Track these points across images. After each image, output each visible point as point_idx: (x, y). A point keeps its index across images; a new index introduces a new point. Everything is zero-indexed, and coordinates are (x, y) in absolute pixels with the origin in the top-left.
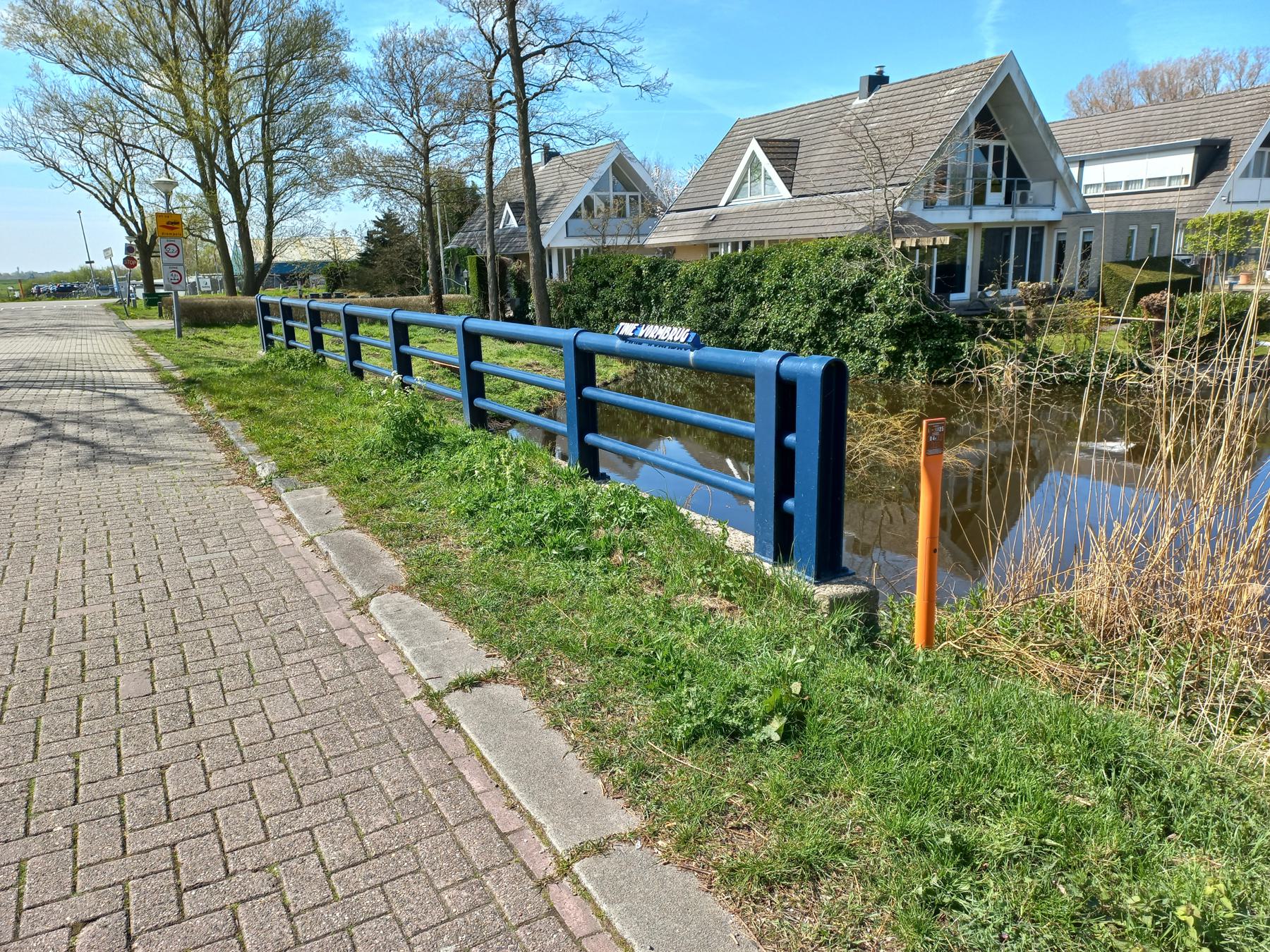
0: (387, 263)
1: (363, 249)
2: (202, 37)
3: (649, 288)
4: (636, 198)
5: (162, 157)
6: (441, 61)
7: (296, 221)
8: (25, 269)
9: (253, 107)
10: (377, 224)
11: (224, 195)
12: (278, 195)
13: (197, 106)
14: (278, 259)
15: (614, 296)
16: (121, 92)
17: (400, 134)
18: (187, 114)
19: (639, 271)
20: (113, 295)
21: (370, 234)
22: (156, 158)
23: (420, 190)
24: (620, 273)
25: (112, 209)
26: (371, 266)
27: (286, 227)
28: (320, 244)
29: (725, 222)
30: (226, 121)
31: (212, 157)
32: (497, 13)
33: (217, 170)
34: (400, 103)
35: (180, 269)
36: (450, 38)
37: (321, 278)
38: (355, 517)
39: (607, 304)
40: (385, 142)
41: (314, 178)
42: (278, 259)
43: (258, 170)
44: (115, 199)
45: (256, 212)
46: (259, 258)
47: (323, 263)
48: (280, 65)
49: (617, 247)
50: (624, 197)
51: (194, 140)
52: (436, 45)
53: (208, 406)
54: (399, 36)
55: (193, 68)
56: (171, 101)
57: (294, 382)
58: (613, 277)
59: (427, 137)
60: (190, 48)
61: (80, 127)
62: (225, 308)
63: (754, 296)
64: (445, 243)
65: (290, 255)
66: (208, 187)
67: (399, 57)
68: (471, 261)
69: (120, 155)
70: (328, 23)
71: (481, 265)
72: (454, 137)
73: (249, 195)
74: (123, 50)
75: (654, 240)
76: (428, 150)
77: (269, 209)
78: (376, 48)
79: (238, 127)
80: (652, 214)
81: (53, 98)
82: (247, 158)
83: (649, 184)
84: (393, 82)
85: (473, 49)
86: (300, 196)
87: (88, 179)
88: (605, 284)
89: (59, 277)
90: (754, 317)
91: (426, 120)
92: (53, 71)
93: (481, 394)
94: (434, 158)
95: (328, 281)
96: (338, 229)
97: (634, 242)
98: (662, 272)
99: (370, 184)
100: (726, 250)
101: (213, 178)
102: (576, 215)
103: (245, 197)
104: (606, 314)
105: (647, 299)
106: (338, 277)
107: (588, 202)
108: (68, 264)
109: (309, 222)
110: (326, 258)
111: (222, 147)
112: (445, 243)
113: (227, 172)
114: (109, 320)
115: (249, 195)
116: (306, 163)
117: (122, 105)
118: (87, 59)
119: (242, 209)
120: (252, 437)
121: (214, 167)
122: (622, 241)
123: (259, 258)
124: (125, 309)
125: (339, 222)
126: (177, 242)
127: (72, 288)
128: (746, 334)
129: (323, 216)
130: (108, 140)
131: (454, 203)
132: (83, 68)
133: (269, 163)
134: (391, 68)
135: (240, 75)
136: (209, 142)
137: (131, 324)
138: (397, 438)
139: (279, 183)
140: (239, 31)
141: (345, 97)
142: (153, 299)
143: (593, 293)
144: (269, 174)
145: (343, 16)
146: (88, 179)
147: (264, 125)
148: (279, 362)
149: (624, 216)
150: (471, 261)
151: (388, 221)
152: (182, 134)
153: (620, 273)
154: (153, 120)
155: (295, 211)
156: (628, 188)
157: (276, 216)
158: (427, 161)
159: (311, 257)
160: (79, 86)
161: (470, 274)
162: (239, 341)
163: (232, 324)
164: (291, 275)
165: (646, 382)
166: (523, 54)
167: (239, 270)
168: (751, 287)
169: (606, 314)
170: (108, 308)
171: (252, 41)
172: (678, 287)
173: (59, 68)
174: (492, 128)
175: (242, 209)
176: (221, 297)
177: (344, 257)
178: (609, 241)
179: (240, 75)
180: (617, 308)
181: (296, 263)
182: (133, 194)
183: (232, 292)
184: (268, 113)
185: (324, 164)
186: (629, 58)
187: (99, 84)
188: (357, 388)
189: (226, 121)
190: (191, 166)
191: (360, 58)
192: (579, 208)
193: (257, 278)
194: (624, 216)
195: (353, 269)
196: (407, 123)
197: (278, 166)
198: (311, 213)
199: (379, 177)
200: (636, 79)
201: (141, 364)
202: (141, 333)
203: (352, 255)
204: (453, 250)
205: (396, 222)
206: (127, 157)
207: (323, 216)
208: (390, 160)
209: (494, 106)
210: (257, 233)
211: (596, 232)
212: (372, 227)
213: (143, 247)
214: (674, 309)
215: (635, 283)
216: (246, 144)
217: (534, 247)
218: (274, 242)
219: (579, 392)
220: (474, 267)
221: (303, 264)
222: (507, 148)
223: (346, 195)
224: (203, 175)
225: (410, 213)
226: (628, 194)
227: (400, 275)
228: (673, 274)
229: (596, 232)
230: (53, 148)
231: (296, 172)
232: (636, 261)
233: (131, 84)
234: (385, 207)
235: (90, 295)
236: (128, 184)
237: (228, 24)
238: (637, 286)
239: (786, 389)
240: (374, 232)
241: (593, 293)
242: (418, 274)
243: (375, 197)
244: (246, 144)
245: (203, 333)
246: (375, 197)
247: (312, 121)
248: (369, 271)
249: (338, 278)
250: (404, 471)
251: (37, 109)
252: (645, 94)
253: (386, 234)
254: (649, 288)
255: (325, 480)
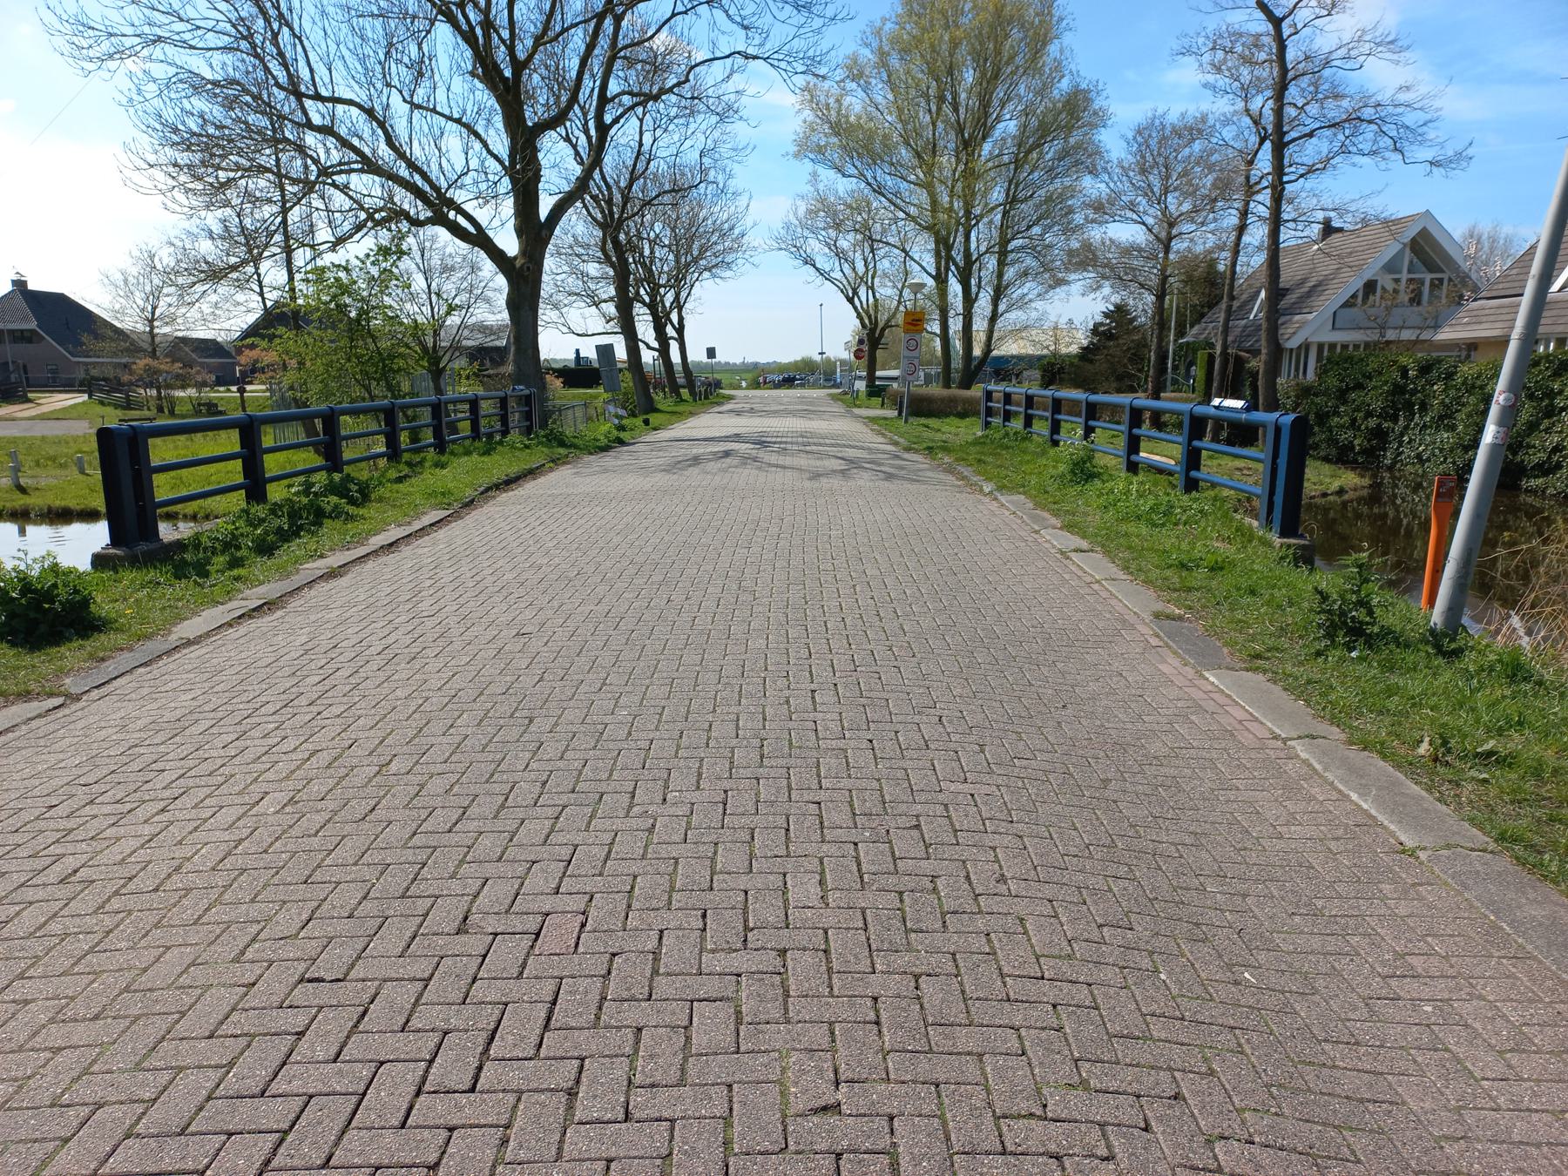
0: (1114, 354)
1: (1085, 343)
2: (960, 130)
3: (1414, 392)
4: (1441, 280)
5: (904, 250)
6: (1197, 146)
7: (1020, 313)
8: (750, 359)
9: (997, 195)
10: (1106, 315)
11: (955, 287)
12: (1007, 286)
13: (945, 199)
14: (995, 353)
15: (1368, 399)
16: (879, 191)
17: (1144, 223)
18: (934, 211)
19: (1404, 371)
20: (834, 386)
21: (1097, 326)
22: (897, 251)
23: (1154, 281)
24: (1380, 373)
25: (851, 300)
26: (1091, 361)
27: (1011, 318)
28: (1042, 337)
29: (1554, 313)
30: (968, 213)
31: (949, 248)
32: (1269, 93)
33: (954, 262)
34: (1148, 191)
35: (916, 362)
36: (1211, 122)
37: (1037, 374)
38: (1037, 505)
39: (1358, 409)
40: (1126, 233)
41: (1047, 268)
42: (995, 353)
43: (991, 263)
44: (855, 292)
45: (983, 304)
46: (977, 352)
47: (1040, 358)
48: (1029, 152)
49: (1399, 342)
50: (1422, 282)
51: (937, 234)
52: (1194, 130)
53: (947, 459)
54: (1157, 122)
55: (946, 161)
56: (923, 197)
57: (1007, 448)
58: (1370, 378)
59: (1171, 225)
60: (949, 142)
61: (838, 226)
62: (942, 400)
63: (1552, 405)
64: (1181, 333)
65: (1009, 348)
66: (940, 279)
67: (1153, 143)
68: (1201, 356)
69: (867, 250)
70: (1088, 100)
71: (1211, 358)
72: (1203, 224)
73: (979, 287)
74: (888, 146)
75: (1445, 334)
76: (1170, 239)
77: (995, 301)
78: (1130, 135)
79: (979, 218)
80: (1458, 301)
81: (822, 200)
82: (983, 249)
83: (1460, 262)
84: (1143, 171)
85: (1237, 135)
86: (1029, 288)
87: (837, 275)
88: (1359, 386)
89: (781, 368)
90: (1547, 430)
91: (1172, 208)
92: (827, 175)
93: (1137, 452)
94: (1177, 245)
95: (1043, 377)
96: (1063, 321)
97: (1425, 336)
98: (1434, 373)
99: (1104, 277)
100: (1547, 347)
101: (947, 269)
102: (1348, 304)
103: (974, 289)
104: (1354, 420)
105: (1409, 406)
106: (1053, 370)
107: (1370, 287)
108: (786, 353)
109: (1034, 315)
110: (1045, 352)
111: (960, 239)
112: (1181, 333)
113: (962, 264)
114: (838, 408)
115: (979, 287)
116: (1038, 251)
117: (877, 203)
118: (858, 164)
119: (969, 300)
120: (979, 473)
121: (949, 258)
122: (1407, 335)
123: (977, 352)
124: (850, 400)
125: (1068, 313)
126: (917, 337)
127: (794, 379)
128: (1531, 451)
129: (1049, 308)
130: (859, 237)
131: (1211, 286)
132: (853, 171)
133: (1003, 255)
134: (1143, 157)
135: (990, 164)
136: (949, 234)
137: (856, 411)
138: (1072, 472)
139: (1010, 273)
140: (998, 119)
141: (1094, 187)
142: (875, 391)
143: (1342, 395)
144: (1002, 263)
145: (1104, 94)
146: (837, 275)
147: (1005, 213)
148: (997, 436)
149: (1419, 304)
150: (1201, 356)
151: (1119, 313)
152: (928, 228)
153: (1380, 373)
154: (902, 215)
155: (1022, 303)
156: (1431, 267)
157: (1002, 307)
158: (1167, 249)
159: (1030, 351)
160: (843, 186)
161: (1198, 371)
162: (953, 430)
163: (947, 416)
164: (1005, 369)
165: (1394, 503)
166: (1287, 138)
167: (957, 363)
168: (1551, 395)
169: (1354, 420)
170: (834, 397)
171: (1008, 127)
172: (1452, 393)
173: (832, 173)
174: (1244, 214)
175: (969, 300)
176: (936, 390)
177: (1064, 351)
178: (1391, 335)
179: (990, 164)
180: (1369, 414)
181: (1013, 357)
182: (872, 288)
183: (947, 385)
184: (1011, 201)
185: (1058, 256)
186: (1420, 130)
187: (863, 185)
188: (1052, 452)
189: (968, 213)
190: (929, 261)
191: (1114, 143)
192: (1354, 296)
193: (973, 371)
194: (1419, 304)
195: (1072, 364)
196: (1152, 211)
197: (1011, 257)
198: (1038, 304)
199: (1112, 269)
200: (1428, 154)
201: (881, 440)
202: (873, 420)
203: (1074, 349)
204: (1188, 343)
205: (1128, 312)
206: (872, 251)
207: (1049, 308)
208: (1129, 250)
209: (1250, 190)
210: (980, 326)
211: (1373, 324)
212: (1099, 318)
213: (872, 340)
214: (1441, 418)
215: (1396, 385)
216: (981, 238)
217: (1268, 341)
218: (996, 335)
219: (1189, 444)
220: (1204, 364)
221: (1020, 358)
222: (1257, 234)
223: (1076, 288)
224: (938, 269)
225: (1142, 305)
226: (1428, 277)
227: (1121, 370)
228: (1450, 376)
229: (1373, 324)
230: (815, 247)
231: (1029, 262)
232: (1403, 360)
233: (890, 182)
234: (1116, 299)
235: (815, 386)
236: (866, 280)
237: (987, 115)
238: (1398, 390)
239: (1278, 429)
240: (1101, 324)
241: (1342, 395)
242: (1140, 371)
243: (1107, 290)
244: (981, 238)
245: (923, 421)
246: (1107, 290)
247: (1055, 210)
248: (1089, 367)
249: (1054, 375)
250: (1073, 491)
251: (809, 212)
252: (1435, 169)
253: (1116, 325)
254: (1414, 392)
255: (1024, 493)
